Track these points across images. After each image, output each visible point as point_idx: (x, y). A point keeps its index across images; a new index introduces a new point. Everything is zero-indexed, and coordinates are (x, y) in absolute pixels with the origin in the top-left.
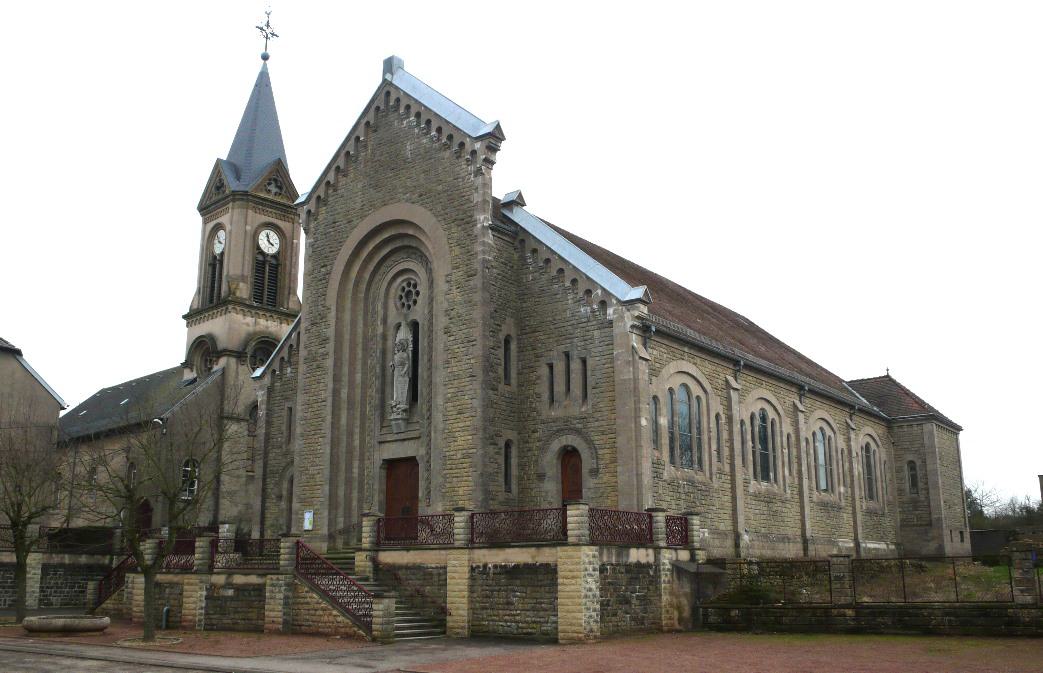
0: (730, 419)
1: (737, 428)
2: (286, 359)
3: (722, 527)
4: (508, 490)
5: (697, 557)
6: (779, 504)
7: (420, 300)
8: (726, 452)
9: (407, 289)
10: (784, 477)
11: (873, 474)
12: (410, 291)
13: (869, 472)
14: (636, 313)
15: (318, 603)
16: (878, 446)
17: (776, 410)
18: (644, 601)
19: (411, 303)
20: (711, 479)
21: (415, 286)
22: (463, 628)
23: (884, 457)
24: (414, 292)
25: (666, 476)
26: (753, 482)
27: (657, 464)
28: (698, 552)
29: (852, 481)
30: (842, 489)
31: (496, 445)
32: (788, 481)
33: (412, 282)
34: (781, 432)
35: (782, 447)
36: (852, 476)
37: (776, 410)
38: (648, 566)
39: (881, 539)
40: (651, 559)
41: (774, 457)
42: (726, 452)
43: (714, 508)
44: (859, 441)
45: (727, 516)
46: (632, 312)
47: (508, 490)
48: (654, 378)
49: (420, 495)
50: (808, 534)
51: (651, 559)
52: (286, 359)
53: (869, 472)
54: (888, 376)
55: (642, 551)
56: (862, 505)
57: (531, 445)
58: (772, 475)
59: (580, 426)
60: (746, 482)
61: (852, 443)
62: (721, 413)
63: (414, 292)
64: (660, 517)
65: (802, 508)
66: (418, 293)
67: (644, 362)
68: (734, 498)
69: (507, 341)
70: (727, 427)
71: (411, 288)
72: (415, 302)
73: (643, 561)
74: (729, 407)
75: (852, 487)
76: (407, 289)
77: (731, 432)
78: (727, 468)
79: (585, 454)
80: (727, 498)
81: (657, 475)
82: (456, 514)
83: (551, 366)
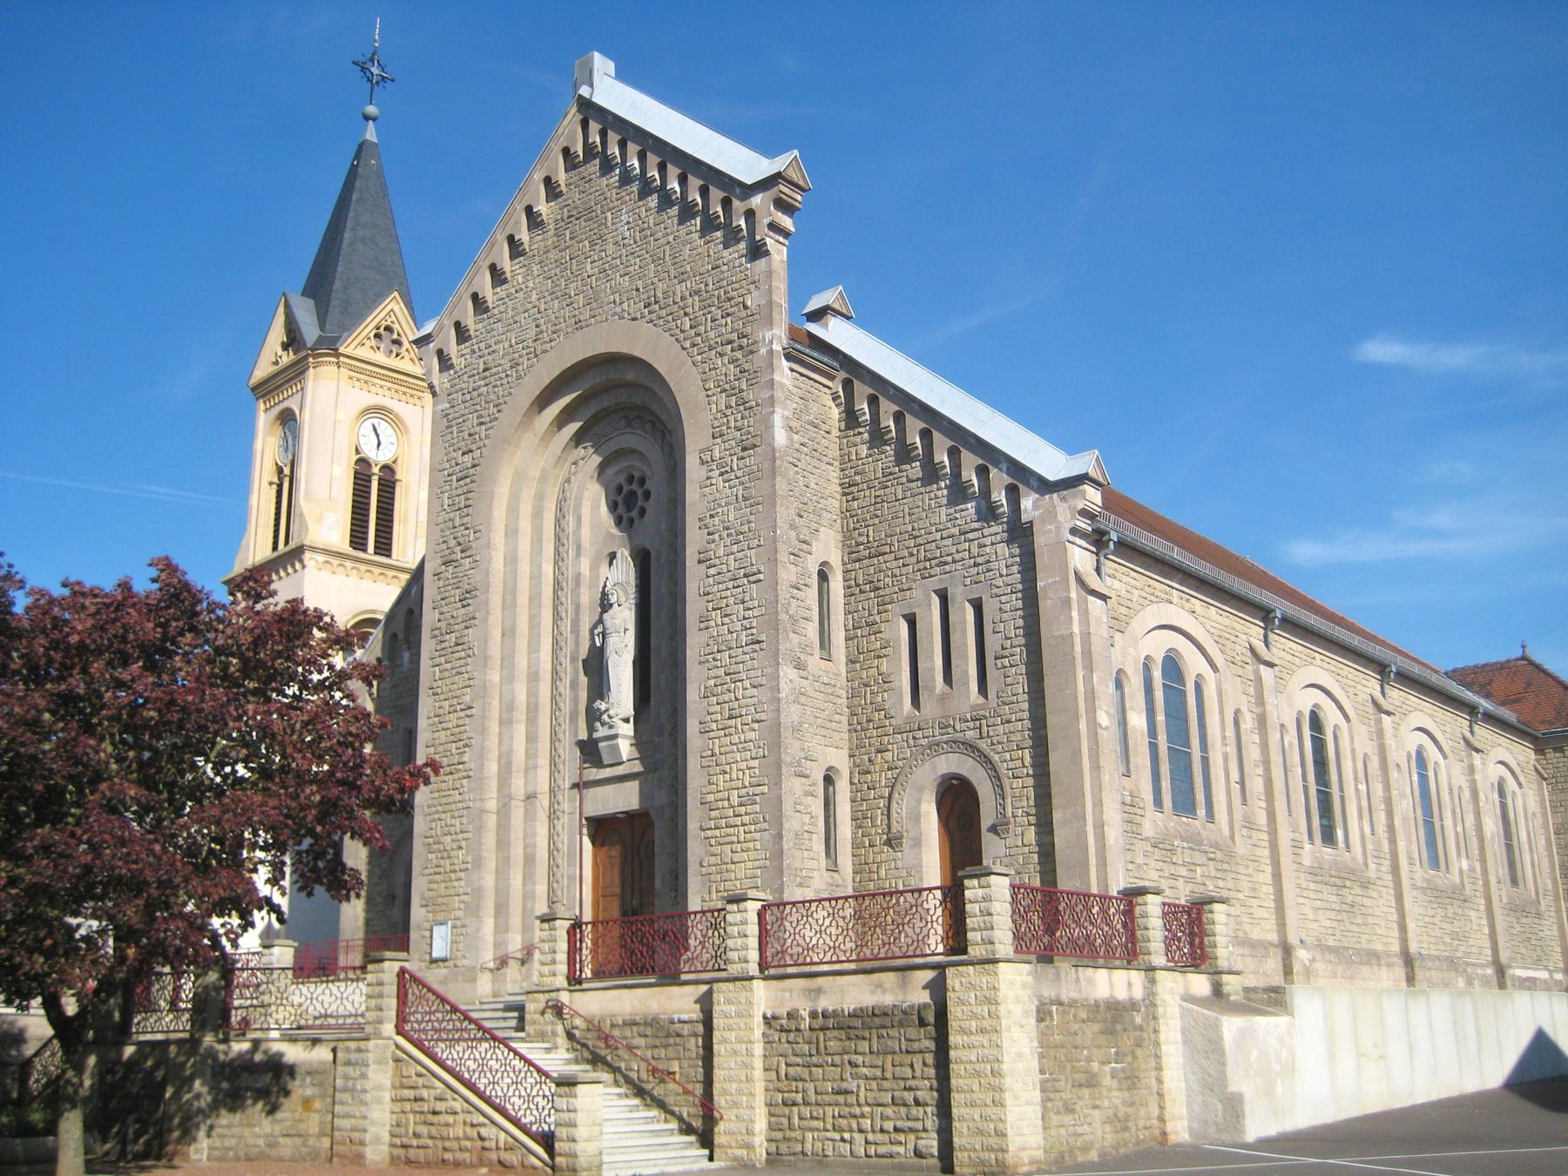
0: (1262, 721)
1: (1274, 737)
2: (401, 636)
3: (1255, 934)
4: (834, 868)
5: (1226, 989)
6: (1358, 890)
7: (651, 506)
8: (1256, 785)
9: (626, 489)
10: (1363, 838)
11: (1514, 837)
12: (633, 494)
13: (1508, 834)
14: (1080, 506)
15: (440, 1099)
16: (1520, 785)
17: (1341, 708)
18: (1130, 1080)
19: (634, 514)
20: (1232, 837)
21: (642, 481)
22: (386, 335)
23: (1533, 805)
24: (640, 492)
25: (1148, 829)
26: (1307, 847)
27: (1130, 807)
28: (1225, 978)
29: (1482, 849)
30: (1465, 865)
31: (806, 777)
32: (1370, 846)
33: (637, 475)
34: (1353, 751)
35: (1356, 779)
36: (1481, 839)
37: (1341, 708)
38: (1133, 1005)
39: (1538, 963)
40: (1138, 993)
41: (1342, 798)
42: (1256, 785)
43: (1240, 896)
44: (1489, 771)
45: (1268, 916)
46: (1072, 502)
47: (834, 868)
48: (1118, 636)
49: (658, 883)
50: (1413, 947)
51: (1138, 993)
52: (401, 636)
53: (1508, 834)
54: (1524, 658)
55: (1120, 976)
56: (1501, 893)
57: (876, 777)
58: (1340, 833)
59: (970, 734)
60: (1297, 845)
61: (1478, 777)
62: (1244, 709)
63: (640, 492)
64: (1152, 907)
65: (1399, 897)
66: (647, 495)
67: (1099, 602)
68: (1277, 877)
69: (823, 576)
70: (1257, 739)
71: (634, 487)
72: (643, 512)
73: (1121, 994)
74: (1260, 700)
75: (1483, 861)
76: (626, 489)
77: (1265, 746)
78: (1262, 818)
79: (985, 790)
80: (1266, 876)
81: (1132, 828)
82: (730, 907)
83: (911, 621)
